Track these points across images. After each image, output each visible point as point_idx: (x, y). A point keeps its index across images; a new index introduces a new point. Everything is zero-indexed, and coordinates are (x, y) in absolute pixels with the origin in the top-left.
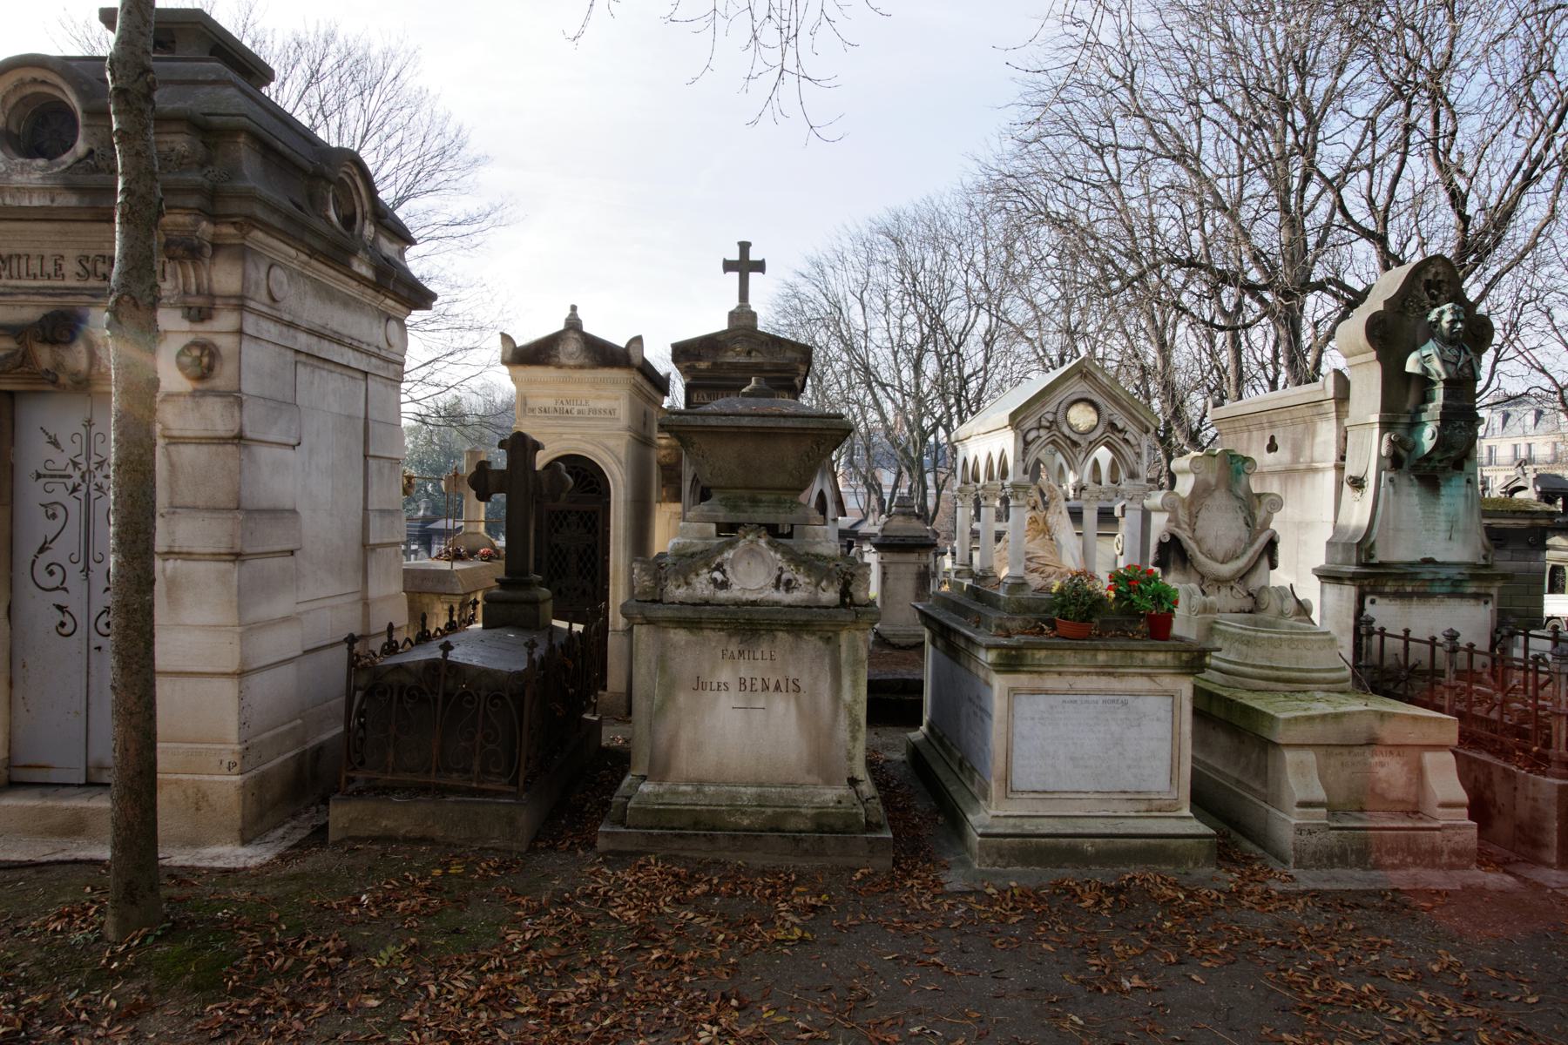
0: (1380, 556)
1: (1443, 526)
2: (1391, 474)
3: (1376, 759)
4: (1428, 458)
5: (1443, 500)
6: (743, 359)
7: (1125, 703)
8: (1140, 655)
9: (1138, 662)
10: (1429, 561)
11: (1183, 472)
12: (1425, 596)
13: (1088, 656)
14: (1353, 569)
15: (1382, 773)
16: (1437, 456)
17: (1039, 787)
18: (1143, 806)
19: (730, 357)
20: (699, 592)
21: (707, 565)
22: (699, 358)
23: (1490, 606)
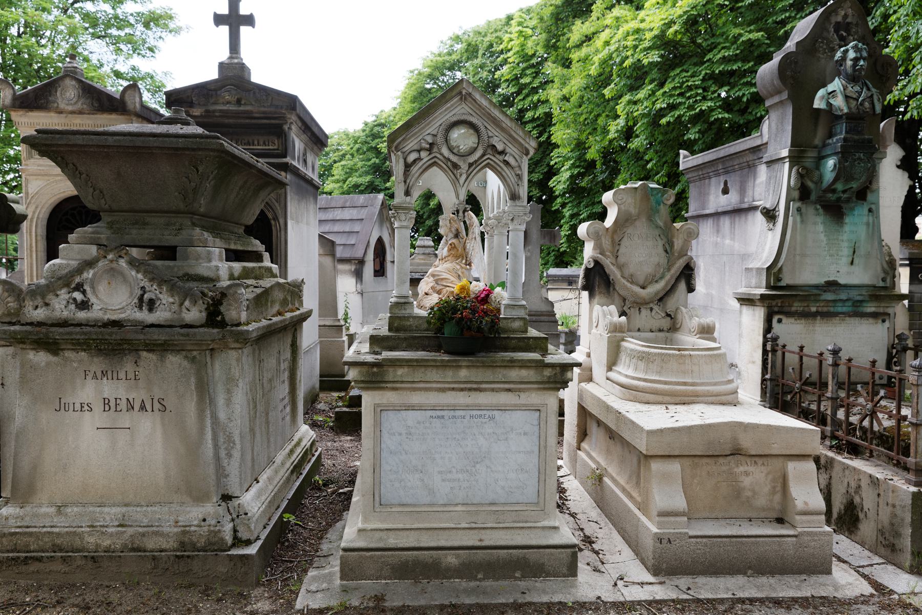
0: (787, 280)
1: (846, 252)
2: (798, 204)
3: (741, 469)
4: (831, 189)
5: (847, 228)
7: (492, 418)
10: (832, 285)
11: (610, 204)
12: (827, 315)
14: (763, 291)
16: (839, 186)
20: (57, 314)
21: (67, 285)
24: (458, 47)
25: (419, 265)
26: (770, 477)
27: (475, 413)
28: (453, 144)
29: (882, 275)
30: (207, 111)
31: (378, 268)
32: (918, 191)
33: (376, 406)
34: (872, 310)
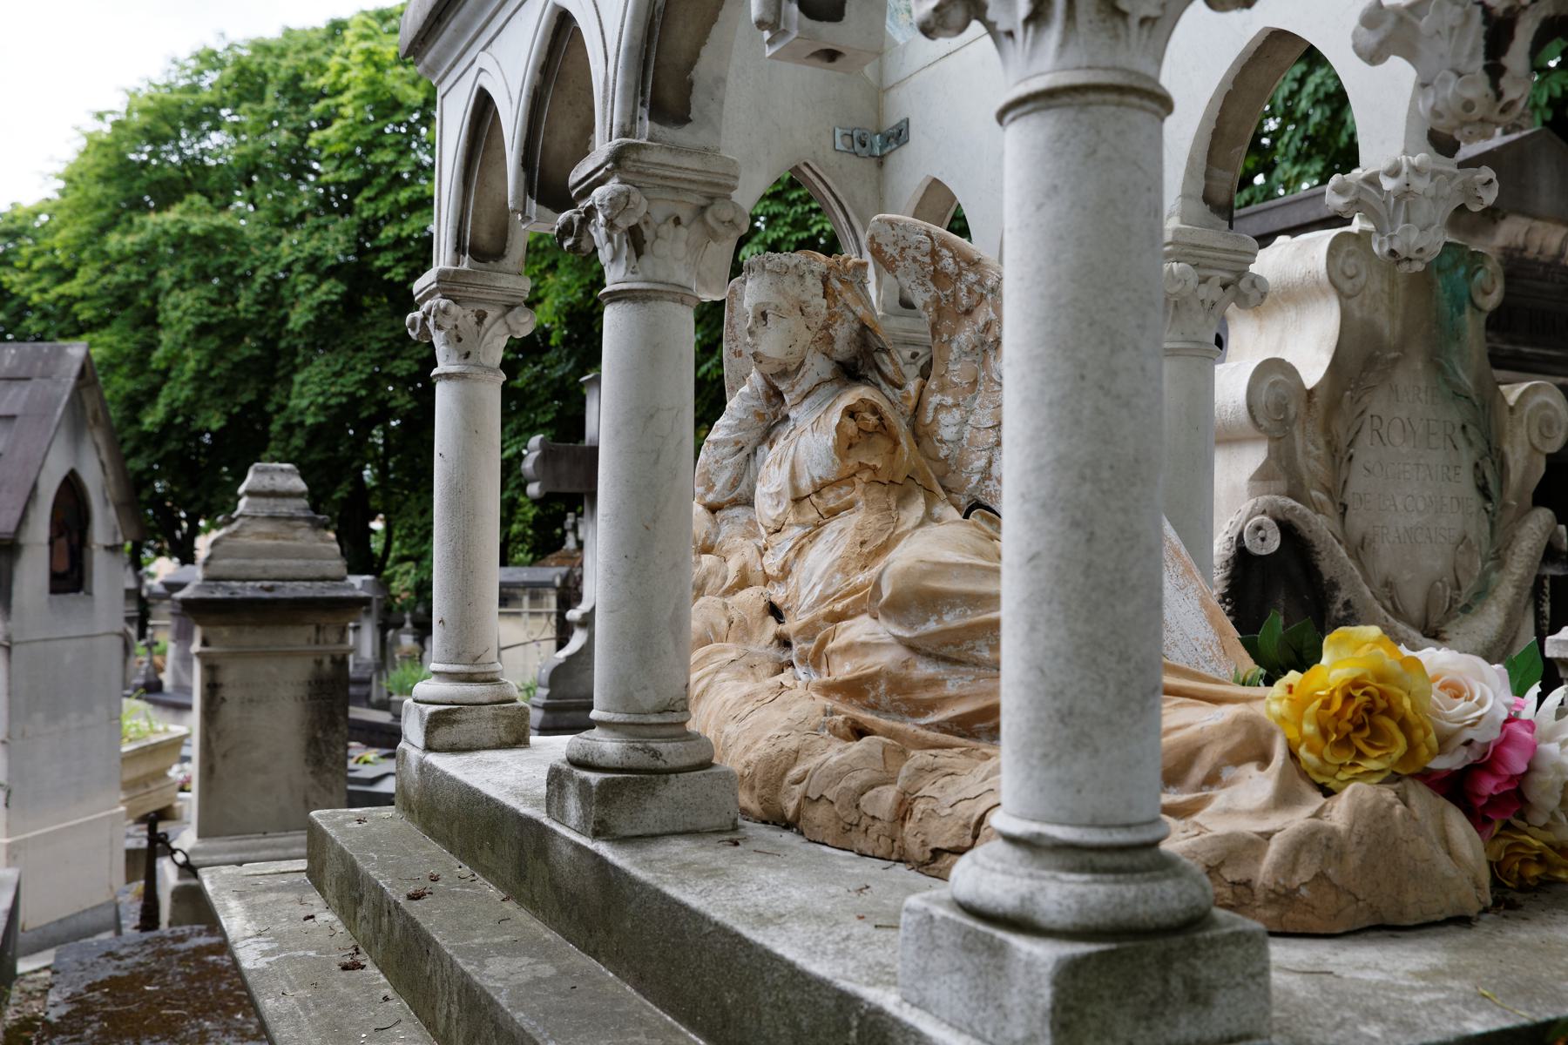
24: (212, 77)
25: (254, 553)
31: (63, 566)
32: (377, 525)
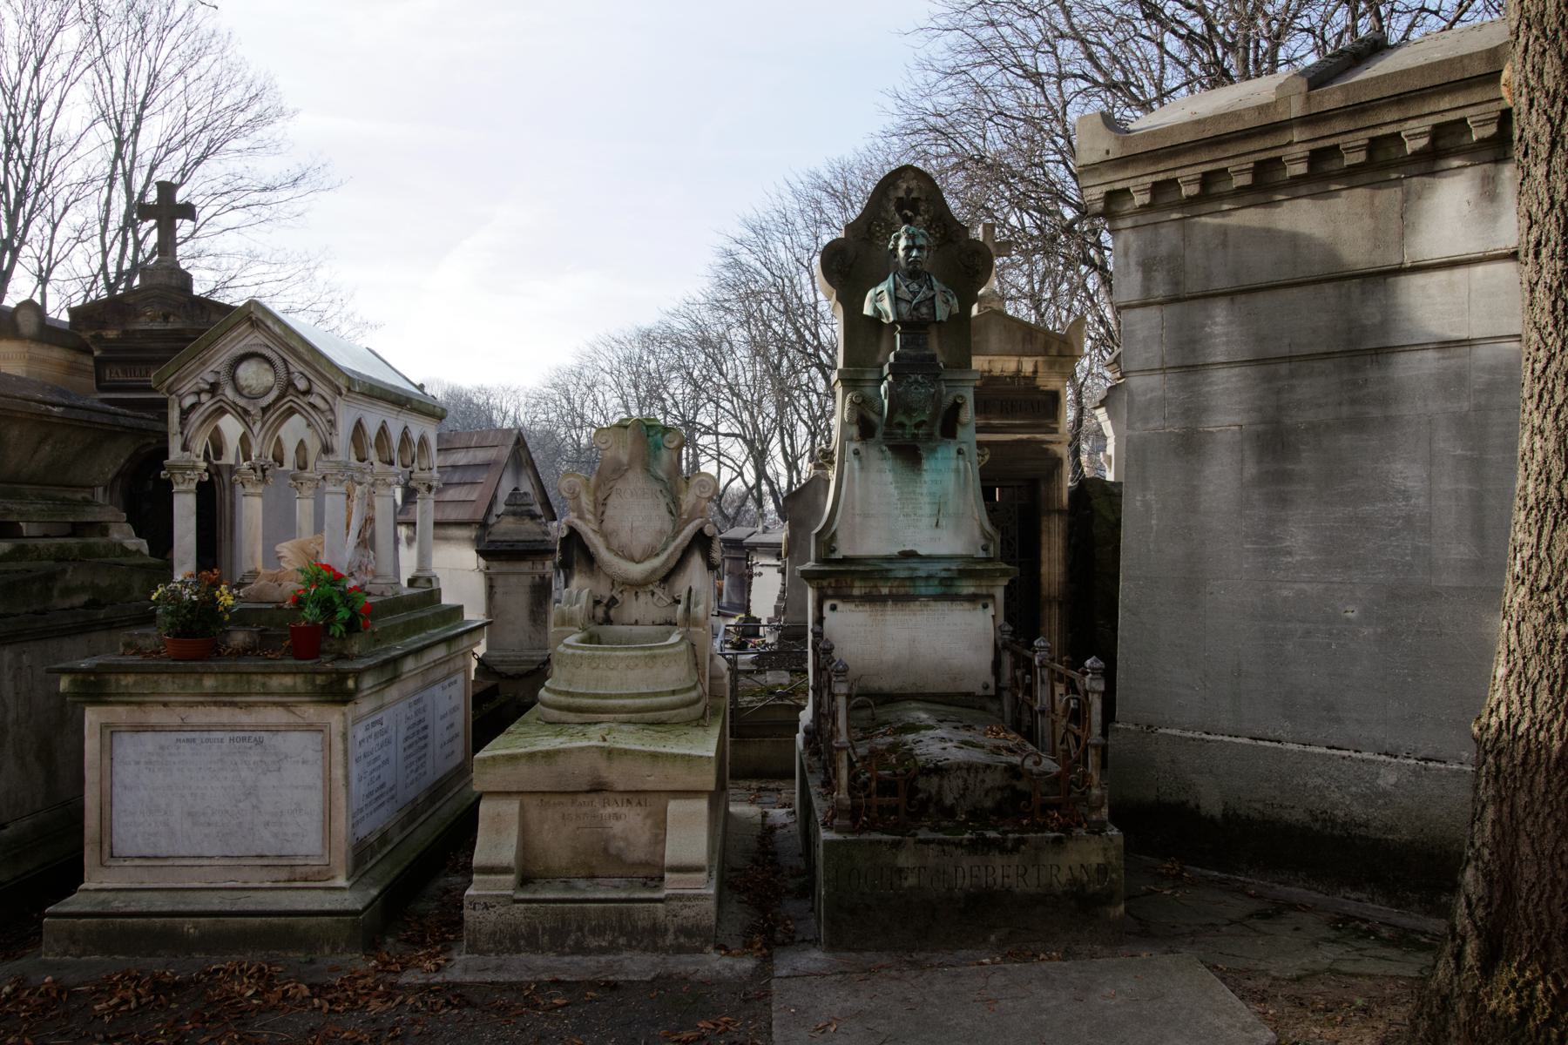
0: (844, 549)
1: (927, 510)
3: (609, 810)
5: (927, 477)
6: (156, 326)
7: (259, 742)
8: (260, 678)
9: (258, 688)
12: (902, 599)
13: (191, 680)
15: (617, 827)
17: (148, 852)
18: (284, 874)
19: (143, 324)
22: (103, 325)
23: (991, 611)
26: (649, 822)
27: (237, 734)
28: (242, 382)
29: (983, 542)
30: (125, 332)
33: (104, 726)
34: (972, 590)
